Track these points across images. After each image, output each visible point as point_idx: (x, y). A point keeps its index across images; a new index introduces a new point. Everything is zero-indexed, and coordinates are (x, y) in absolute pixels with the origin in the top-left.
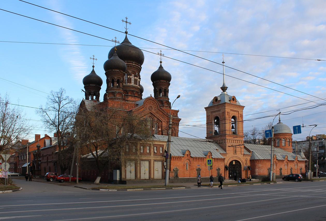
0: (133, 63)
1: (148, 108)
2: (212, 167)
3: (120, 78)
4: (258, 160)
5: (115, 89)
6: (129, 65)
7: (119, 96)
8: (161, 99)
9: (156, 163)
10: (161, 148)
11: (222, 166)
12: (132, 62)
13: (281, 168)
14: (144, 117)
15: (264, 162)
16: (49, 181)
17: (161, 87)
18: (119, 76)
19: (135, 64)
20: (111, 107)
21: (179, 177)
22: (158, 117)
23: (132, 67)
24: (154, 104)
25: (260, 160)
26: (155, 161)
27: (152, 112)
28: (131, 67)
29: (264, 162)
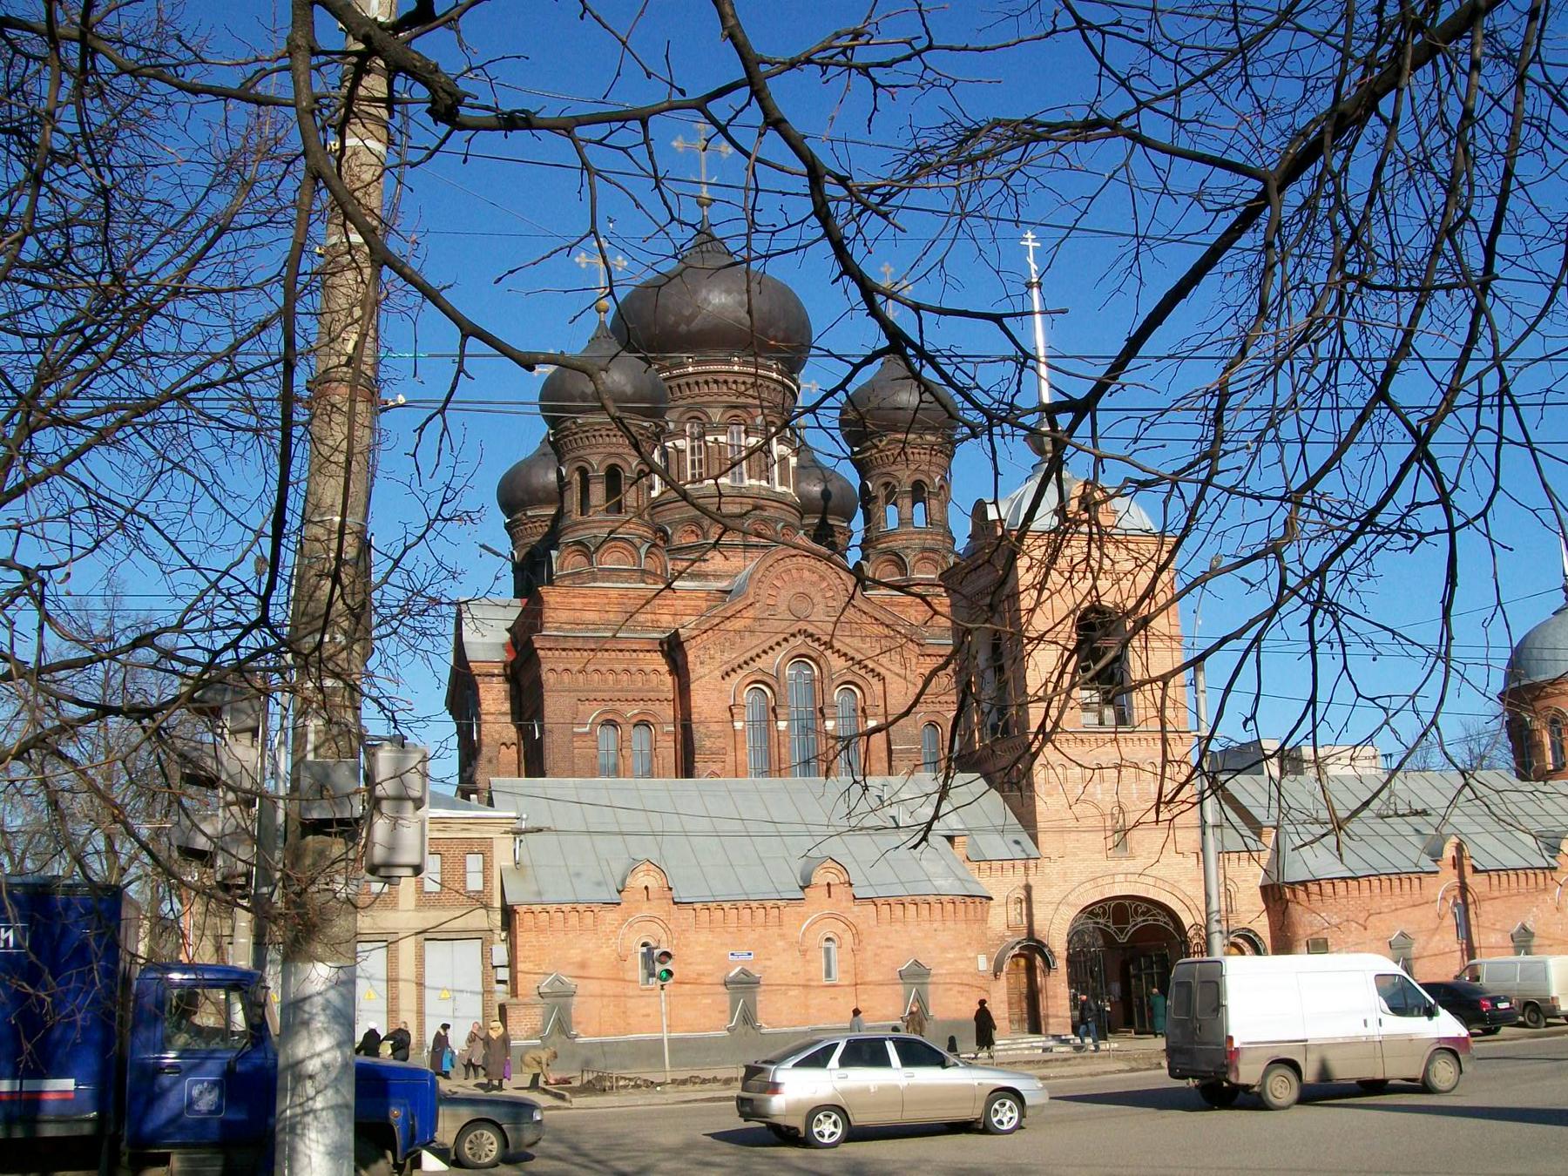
0: (729, 363)
1: (784, 607)
2: (668, 966)
3: (619, 455)
4: (1304, 883)
5: (594, 521)
6: (709, 378)
7: (619, 561)
8: (896, 544)
9: (436, 953)
10: (474, 863)
11: (944, 950)
12: (721, 355)
13: (1524, 928)
14: (759, 664)
15: (1397, 891)
16: (988, 1014)
17: (889, 474)
18: (612, 450)
19: (698, 363)
20: (557, 629)
21: (576, 1036)
22: (858, 651)
23: (697, 383)
24: (823, 578)
25: (1317, 881)
26: (426, 935)
28: (684, 388)
29: (1397, 891)
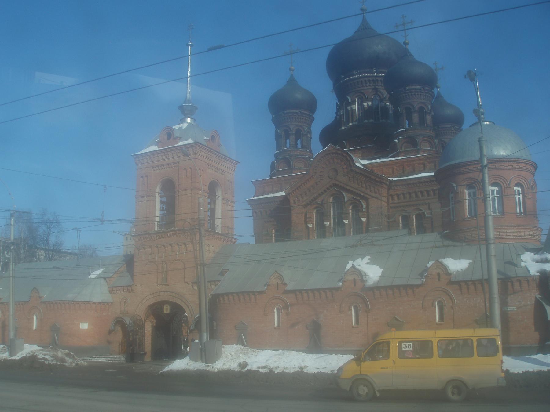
27: (337, 183)
